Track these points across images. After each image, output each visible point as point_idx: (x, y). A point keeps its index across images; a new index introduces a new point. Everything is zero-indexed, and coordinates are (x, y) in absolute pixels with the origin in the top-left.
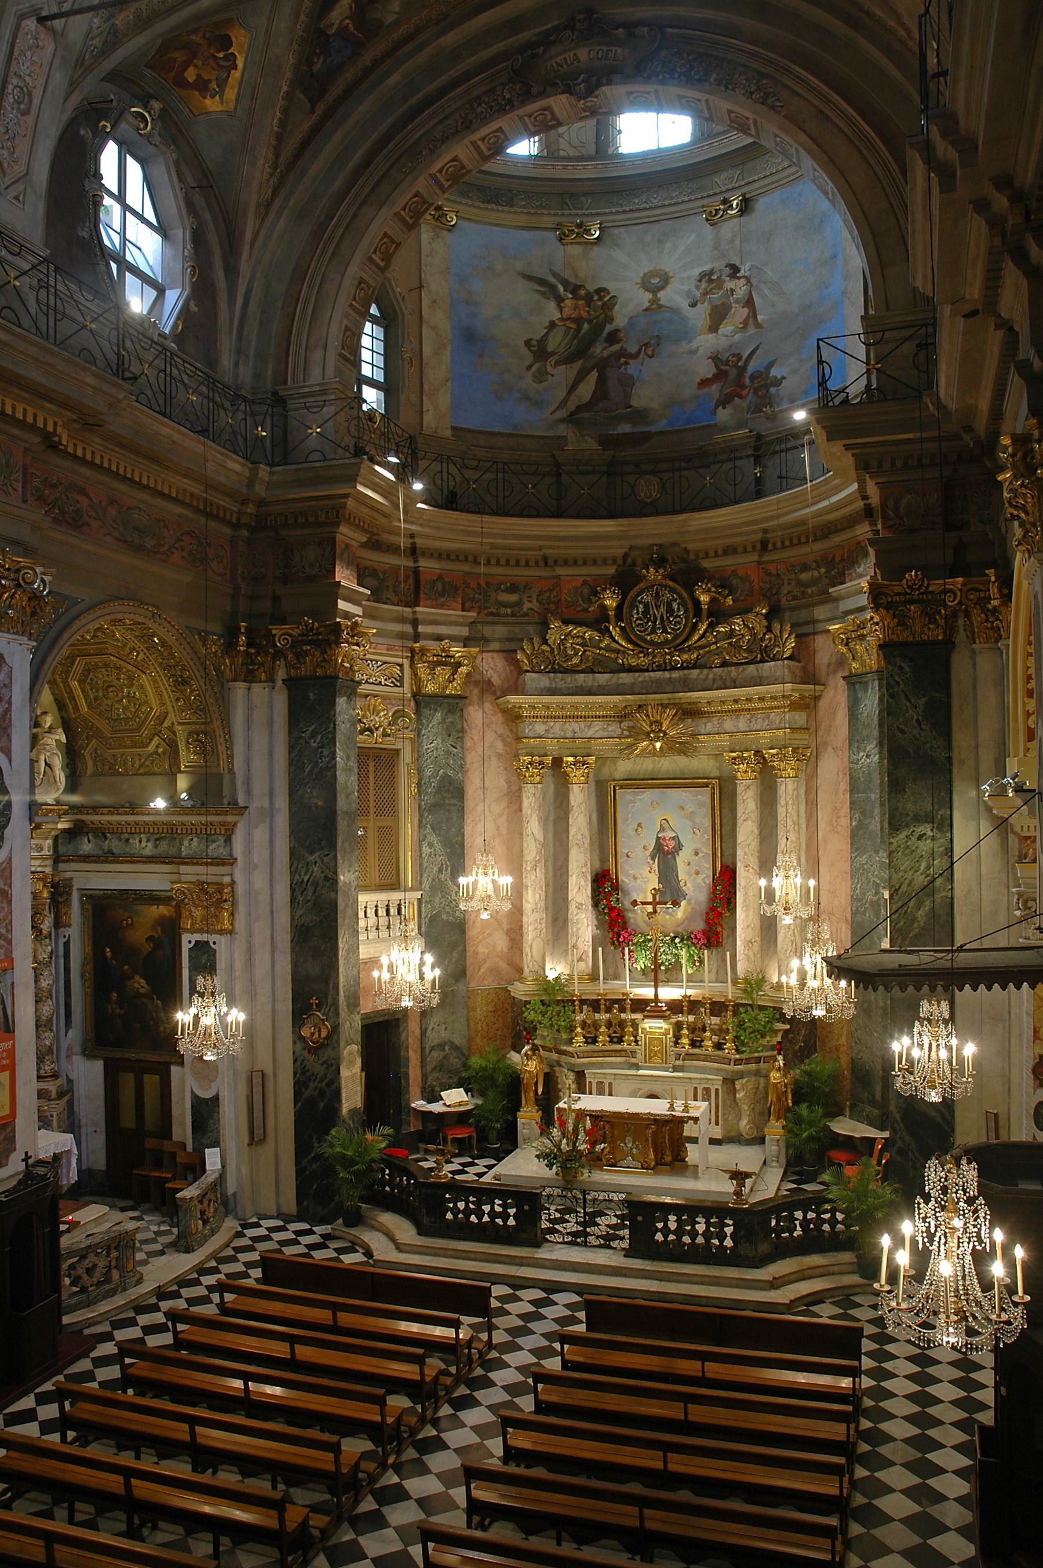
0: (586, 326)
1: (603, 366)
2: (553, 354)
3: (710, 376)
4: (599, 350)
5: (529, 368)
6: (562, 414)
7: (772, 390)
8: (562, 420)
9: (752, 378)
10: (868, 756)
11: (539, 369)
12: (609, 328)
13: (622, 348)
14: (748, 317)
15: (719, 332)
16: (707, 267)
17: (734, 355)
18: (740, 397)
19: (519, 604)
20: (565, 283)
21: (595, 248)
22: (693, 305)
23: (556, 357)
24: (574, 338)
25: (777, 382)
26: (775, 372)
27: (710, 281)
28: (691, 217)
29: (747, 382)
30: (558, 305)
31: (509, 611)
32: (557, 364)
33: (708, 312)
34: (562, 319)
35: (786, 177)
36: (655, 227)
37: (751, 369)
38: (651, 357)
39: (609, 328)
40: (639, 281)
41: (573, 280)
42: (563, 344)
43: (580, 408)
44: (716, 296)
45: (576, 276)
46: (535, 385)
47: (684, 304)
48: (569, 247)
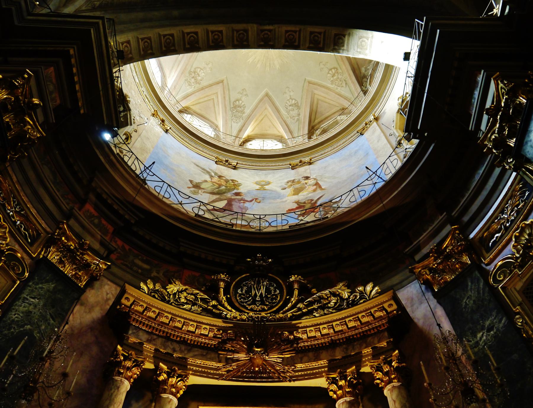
3: (294, 208)
4: (229, 195)
5: (189, 188)
10: (489, 330)
12: (235, 191)
13: (242, 198)
14: (316, 188)
16: (292, 179)
20: (216, 174)
22: (285, 189)
23: (205, 190)
30: (210, 177)
31: (140, 271)
44: (297, 186)
47: (279, 190)
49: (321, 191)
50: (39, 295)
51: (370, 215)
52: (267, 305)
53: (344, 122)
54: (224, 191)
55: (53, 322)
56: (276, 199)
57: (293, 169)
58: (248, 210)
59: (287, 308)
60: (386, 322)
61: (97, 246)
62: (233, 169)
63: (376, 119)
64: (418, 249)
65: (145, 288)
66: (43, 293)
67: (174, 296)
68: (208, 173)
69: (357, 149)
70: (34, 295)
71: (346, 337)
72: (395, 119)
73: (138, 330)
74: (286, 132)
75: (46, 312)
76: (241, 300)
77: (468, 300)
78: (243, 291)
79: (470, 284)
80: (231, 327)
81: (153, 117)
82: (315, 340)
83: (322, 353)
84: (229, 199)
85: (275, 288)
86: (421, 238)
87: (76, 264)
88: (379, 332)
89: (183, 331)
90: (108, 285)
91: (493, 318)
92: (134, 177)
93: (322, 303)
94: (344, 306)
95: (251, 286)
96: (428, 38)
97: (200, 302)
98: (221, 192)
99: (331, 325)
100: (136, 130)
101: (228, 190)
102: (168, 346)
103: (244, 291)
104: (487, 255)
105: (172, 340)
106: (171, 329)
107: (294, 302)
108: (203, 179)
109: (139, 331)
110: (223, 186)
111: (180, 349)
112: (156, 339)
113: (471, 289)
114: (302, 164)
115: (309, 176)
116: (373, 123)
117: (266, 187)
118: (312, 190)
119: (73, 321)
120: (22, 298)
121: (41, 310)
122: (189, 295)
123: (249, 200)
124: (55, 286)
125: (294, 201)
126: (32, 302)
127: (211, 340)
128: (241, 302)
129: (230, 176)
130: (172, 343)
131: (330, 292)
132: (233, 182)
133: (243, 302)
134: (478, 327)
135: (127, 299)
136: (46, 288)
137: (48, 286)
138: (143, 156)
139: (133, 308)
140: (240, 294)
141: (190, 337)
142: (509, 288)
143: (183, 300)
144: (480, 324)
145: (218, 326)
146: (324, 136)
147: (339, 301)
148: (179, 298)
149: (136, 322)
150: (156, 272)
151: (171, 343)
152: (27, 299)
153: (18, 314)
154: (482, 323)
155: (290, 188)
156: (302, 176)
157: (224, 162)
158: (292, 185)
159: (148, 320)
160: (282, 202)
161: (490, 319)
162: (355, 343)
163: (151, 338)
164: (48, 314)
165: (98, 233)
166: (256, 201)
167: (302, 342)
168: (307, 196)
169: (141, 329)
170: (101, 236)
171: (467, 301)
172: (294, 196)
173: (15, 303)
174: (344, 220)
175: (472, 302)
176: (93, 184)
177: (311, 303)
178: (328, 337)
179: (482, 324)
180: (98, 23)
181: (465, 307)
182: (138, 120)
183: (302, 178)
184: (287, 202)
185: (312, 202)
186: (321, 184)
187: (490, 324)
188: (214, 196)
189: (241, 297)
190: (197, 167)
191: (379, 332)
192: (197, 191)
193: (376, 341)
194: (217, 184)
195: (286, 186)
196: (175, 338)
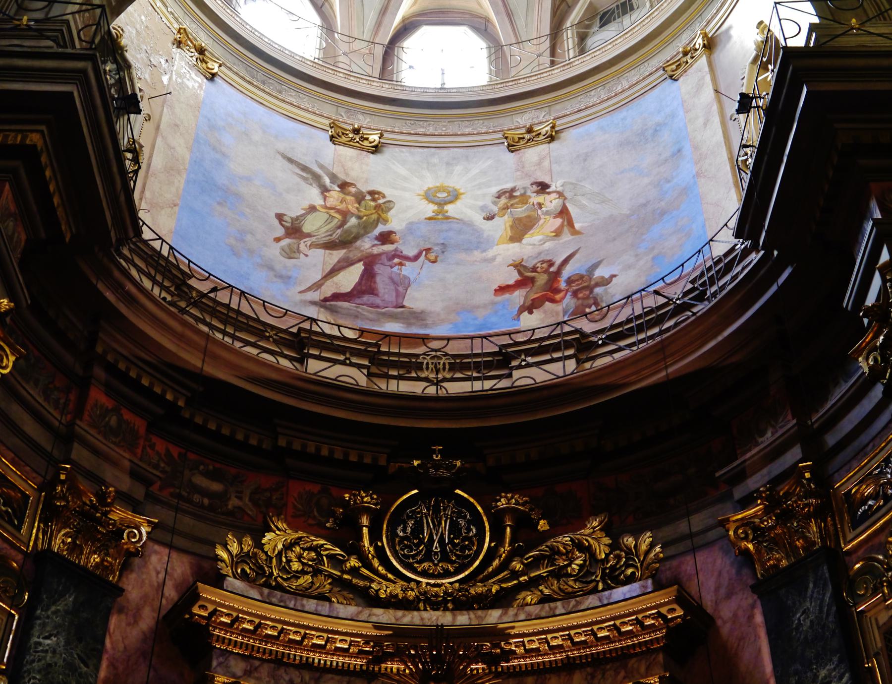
0: (353, 221)
1: (370, 262)
2: (309, 235)
4: (367, 244)
5: (278, 240)
6: (316, 296)
7: (597, 290)
8: (314, 303)
9: (569, 281)
11: (289, 245)
12: (381, 228)
13: (396, 250)
14: (562, 226)
15: (524, 241)
16: (508, 186)
17: (543, 262)
18: (553, 301)
19: (222, 497)
20: (333, 177)
21: (371, 156)
22: (490, 218)
23: (313, 239)
24: (339, 227)
25: (605, 282)
26: (601, 272)
27: (511, 197)
29: (563, 285)
30: (322, 193)
31: (206, 501)
35: (604, 109)
36: (444, 152)
37: (567, 272)
38: (434, 262)
40: (422, 193)
43: (337, 297)
44: (520, 211)
46: (282, 259)
47: (478, 219)
48: (341, 148)
49: (571, 237)
50: (56, 627)
51: (658, 379)
52: (452, 562)
54: (355, 231)
55: (86, 669)
56: (472, 250)
57: (512, 152)
59: (490, 569)
60: (662, 636)
61: (125, 483)
62: (372, 153)
63: (710, 45)
64: (741, 476)
65: (225, 556)
66: (60, 622)
67: (278, 557)
68: (317, 178)
69: (659, 118)
70: (48, 632)
71: (592, 654)
72: (746, 75)
73: (227, 655)
74: (497, 13)
75: (71, 655)
76: (403, 551)
77: (803, 616)
78: (406, 530)
79: (811, 585)
80: (390, 635)
81: (179, 50)
82: (538, 656)
83: (550, 679)
84: (367, 257)
85: (469, 523)
86: (748, 455)
87: (99, 540)
88: (649, 652)
89: (304, 646)
90: (156, 552)
91: (832, 667)
92: (174, 313)
93: (557, 565)
94: (597, 577)
95: (421, 518)
96: (785, 91)
97: (326, 565)
98: (349, 238)
99: (567, 635)
100: (149, 115)
101: (366, 228)
102: (282, 677)
103: (409, 530)
104: (850, 536)
105: (287, 665)
106: (283, 646)
107: (504, 555)
108: (306, 205)
109: (228, 657)
111: (302, 681)
112: (259, 666)
113: (812, 596)
114: (531, 136)
115: (547, 180)
116: (700, 56)
117: (450, 209)
118: (553, 229)
119: (113, 648)
120: (33, 646)
121: (64, 655)
122: (307, 552)
123: (411, 253)
124: (75, 598)
125: (511, 262)
126: (48, 645)
127: (355, 657)
128: (404, 555)
129: (367, 181)
130: (287, 669)
131: (572, 540)
132: (374, 200)
133: (407, 557)
134: (809, 674)
135: (203, 607)
136: (62, 609)
137: (65, 603)
139: (215, 621)
140: (401, 537)
141: (317, 655)
142: (868, 617)
143: (296, 566)
144: (811, 670)
145: (366, 636)
146: (588, 58)
147: (588, 563)
148: (289, 561)
149: (221, 642)
150: (236, 497)
151: (285, 671)
152: (40, 644)
153: (34, 678)
154: (816, 669)
156: (533, 180)
157: (351, 135)
158: (507, 208)
159: (243, 636)
160: (486, 260)
161: (828, 667)
162: (608, 667)
163: (251, 666)
164: (76, 656)
165: (124, 457)
167: (515, 659)
169: (232, 653)
170: (130, 461)
171: (802, 618)
172: (512, 245)
173: (26, 660)
174: (612, 379)
175: (808, 623)
176: (99, 349)
177: (537, 562)
178: (562, 652)
179: (814, 671)
180: (84, 72)
181: (797, 629)
182: (149, 81)
183: (532, 184)
184: (495, 263)
185: (552, 269)
186: (572, 214)
187: (825, 677)
188: (335, 252)
189: (404, 544)
190: (290, 166)
191: (649, 652)
193: (643, 669)
194: (338, 211)
195: (495, 209)
196: (291, 661)
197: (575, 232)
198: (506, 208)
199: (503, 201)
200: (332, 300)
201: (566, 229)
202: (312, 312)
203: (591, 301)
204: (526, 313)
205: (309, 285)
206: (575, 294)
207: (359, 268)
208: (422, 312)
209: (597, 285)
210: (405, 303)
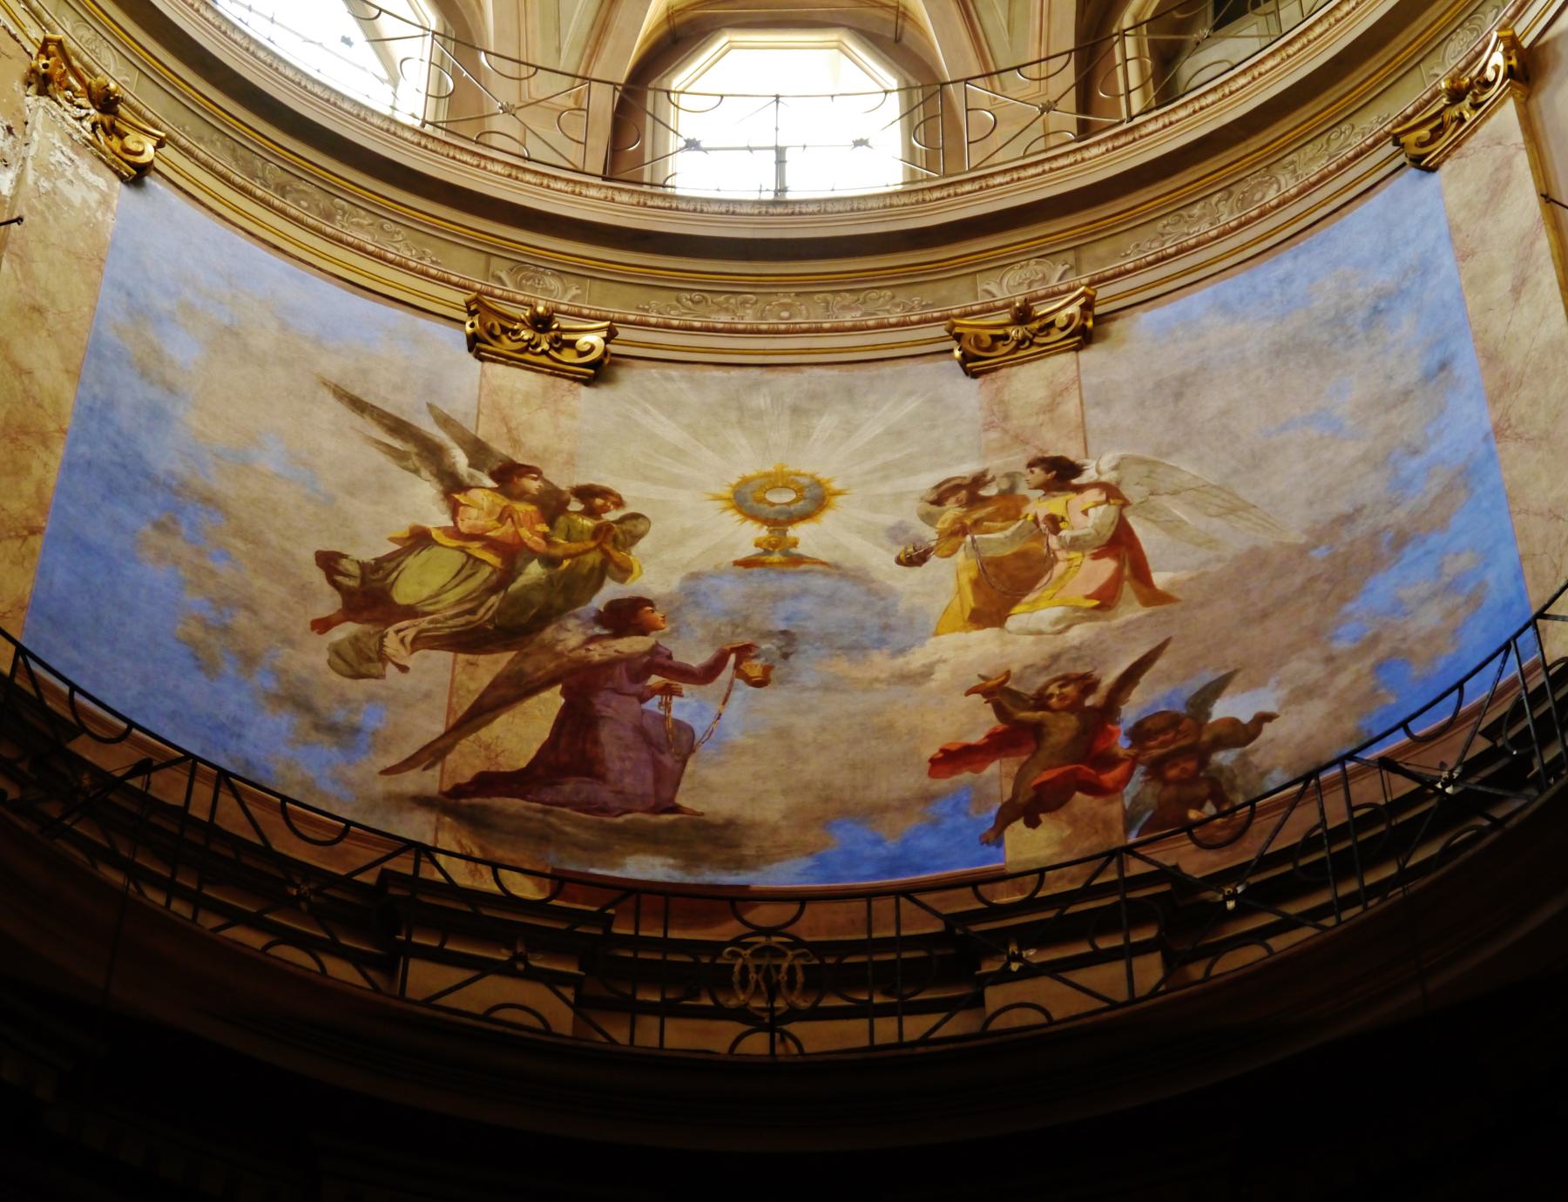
0: (534, 571)
2: (411, 612)
3: (977, 737)
4: (571, 636)
5: (322, 625)
6: (428, 781)
8: (422, 801)
9: (1140, 733)
11: (355, 641)
12: (611, 591)
13: (655, 650)
14: (1116, 581)
15: (1011, 623)
17: (1066, 680)
18: (1096, 790)
20: (478, 451)
22: (915, 558)
23: (424, 623)
24: (493, 590)
25: (1242, 734)
26: (1230, 707)
27: (974, 501)
28: (904, 364)
29: (1122, 745)
32: (422, 642)
33: (965, 578)
34: (455, 533)
36: (786, 381)
37: (1133, 709)
38: (760, 684)
39: (611, 591)
40: (726, 492)
41: (502, 448)
42: (451, 597)
43: (489, 782)
44: (999, 539)
45: (516, 443)
46: (335, 677)
47: (881, 561)
53: (1318, 30)
58: (692, 750)
68: (432, 454)
69: (1384, 278)
81: (44, 100)
108: (402, 527)
110: (532, 554)
115: (1072, 453)
116: (1499, 102)
118: (1092, 588)
123: (698, 658)
125: (977, 682)
129: (571, 461)
132: (591, 512)
138: (28, 487)
146: (1182, 113)
155: (954, 551)
156: (1033, 453)
157: (526, 335)
166: (745, 666)
168: (1059, 643)
172: (977, 635)
184: (932, 685)
185: (1090, 701)
186: (1145, 547)
188: (482, 659)
192: (373, 643)
194: (492, 544)
195: (930, 534)
197: (1153, 597)
198: (960, 530)
199: (951, 511)
200: (475, 794)
201: (1127, 589)
202: (417, 827)
203: (1203, 790)
204: (1019, 825)
205: (409, 750)
206: (1156, 769)
207: (551, 702)
208: (730, 823)
209: (1220, 743)
210: (682, 800)
